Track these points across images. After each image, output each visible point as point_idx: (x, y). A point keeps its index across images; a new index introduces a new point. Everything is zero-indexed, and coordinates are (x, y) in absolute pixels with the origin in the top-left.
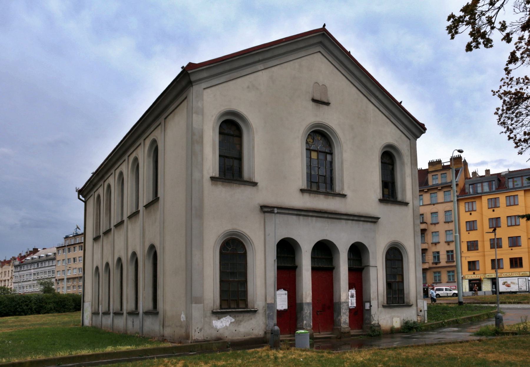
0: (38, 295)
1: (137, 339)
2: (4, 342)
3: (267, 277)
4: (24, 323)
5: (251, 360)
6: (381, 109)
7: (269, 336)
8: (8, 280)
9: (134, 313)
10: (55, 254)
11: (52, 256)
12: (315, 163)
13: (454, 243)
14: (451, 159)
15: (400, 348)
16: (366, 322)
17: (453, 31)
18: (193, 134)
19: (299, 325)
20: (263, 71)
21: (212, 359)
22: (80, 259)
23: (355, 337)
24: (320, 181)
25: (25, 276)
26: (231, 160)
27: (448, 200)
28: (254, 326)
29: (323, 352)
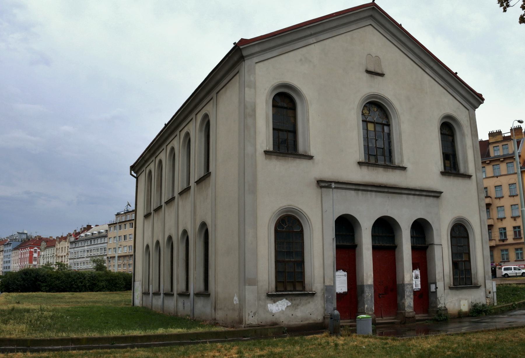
0: (92, 273)
1: (189, 322)
2: (63, 317)
4: (79, 300)
5: (310, 347)
6: (437, 79)
7: (328, 321)
8: (65, 256)
9: (185, 294)
10: (107, 231)
11: (104, 234)
12: (372, 135)
13: (521, 218)
14: (511, 130)
15: (469, 334)
16: (432, 305)
17: (505, 4)
18: (245, 107)
19: (359, 310)
21: (268, 345)
22: (131, 236)
23: (421, 322)
24: (378, 154)
25: (79, 253)
26: (285, 133)
27: (512, 172)
28: (312, 310)
29: (387, 339)
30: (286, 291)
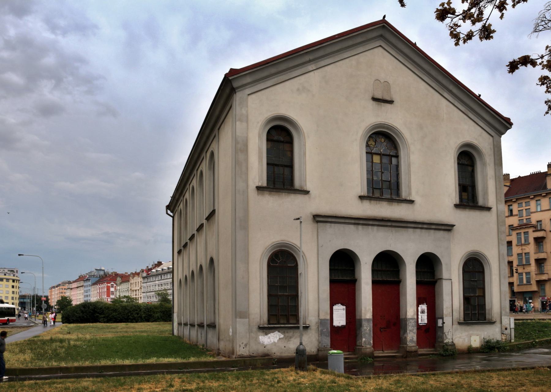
3: (320, 291)
12: (377, 168)
16: (439, 340)
20: (315, 71)
23: (424, 357)
26: (281, 168)
30: (279, 324)
